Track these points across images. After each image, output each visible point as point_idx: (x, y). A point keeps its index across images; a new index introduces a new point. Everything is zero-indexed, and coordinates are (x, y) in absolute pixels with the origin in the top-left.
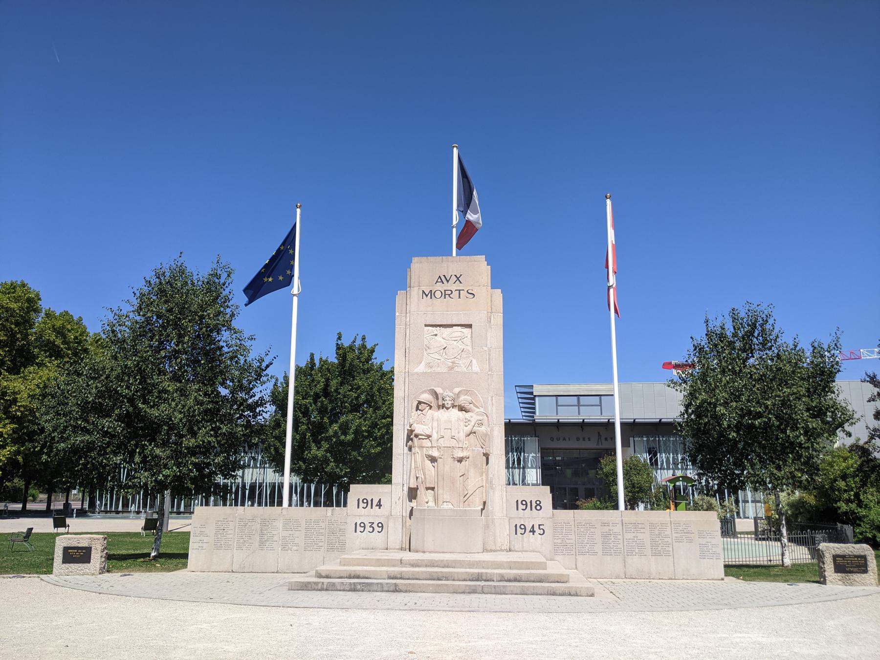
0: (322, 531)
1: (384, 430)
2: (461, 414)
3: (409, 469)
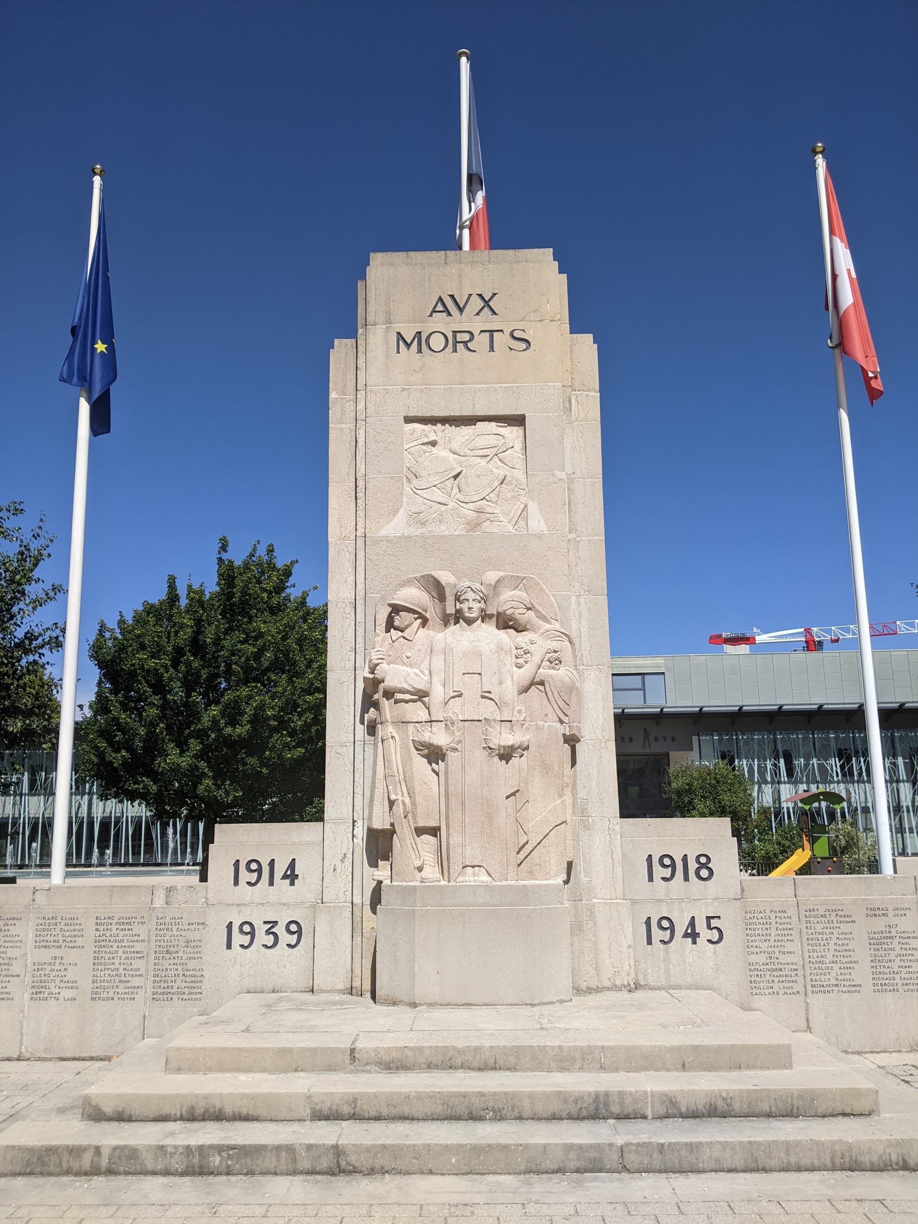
0: (138, 947)
1: (309, 716)
2: (506, 637)
3: (368, 780)
